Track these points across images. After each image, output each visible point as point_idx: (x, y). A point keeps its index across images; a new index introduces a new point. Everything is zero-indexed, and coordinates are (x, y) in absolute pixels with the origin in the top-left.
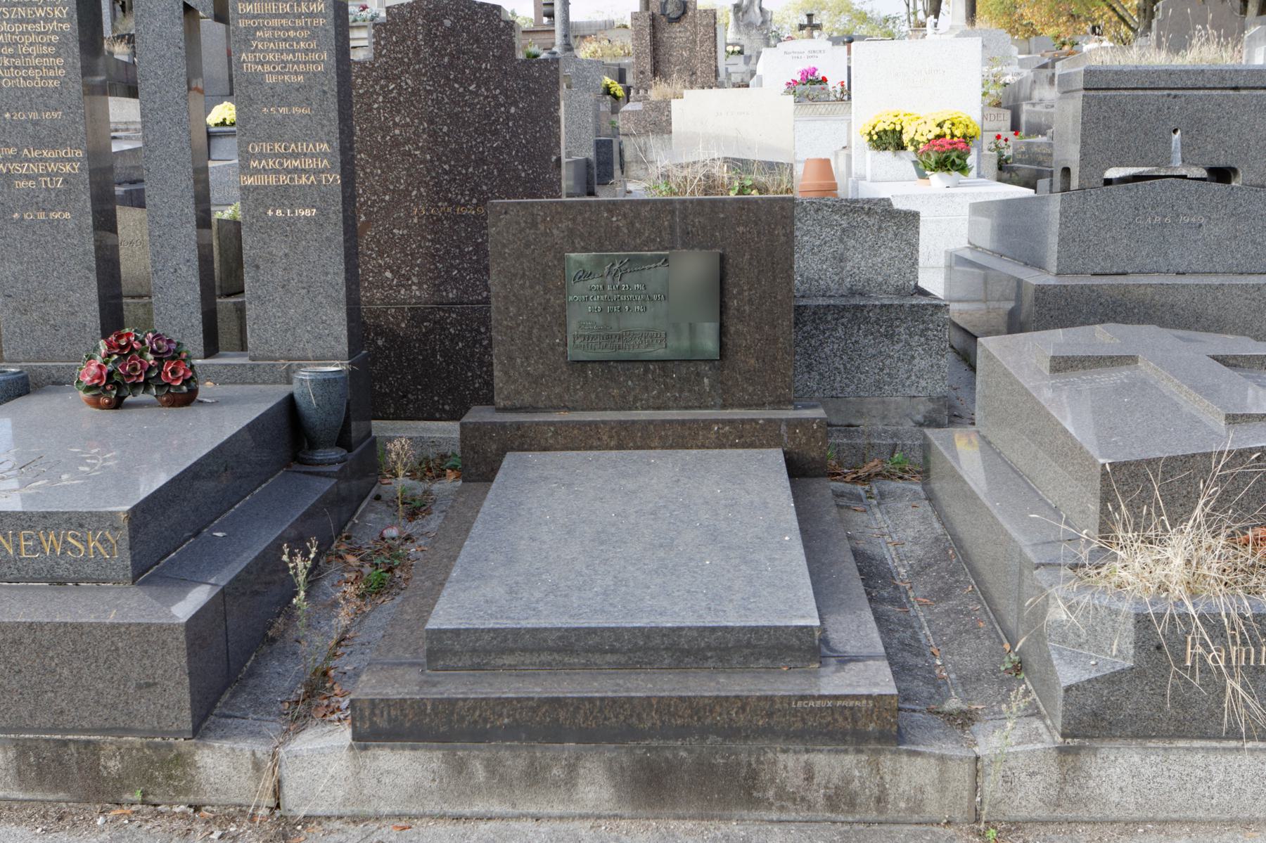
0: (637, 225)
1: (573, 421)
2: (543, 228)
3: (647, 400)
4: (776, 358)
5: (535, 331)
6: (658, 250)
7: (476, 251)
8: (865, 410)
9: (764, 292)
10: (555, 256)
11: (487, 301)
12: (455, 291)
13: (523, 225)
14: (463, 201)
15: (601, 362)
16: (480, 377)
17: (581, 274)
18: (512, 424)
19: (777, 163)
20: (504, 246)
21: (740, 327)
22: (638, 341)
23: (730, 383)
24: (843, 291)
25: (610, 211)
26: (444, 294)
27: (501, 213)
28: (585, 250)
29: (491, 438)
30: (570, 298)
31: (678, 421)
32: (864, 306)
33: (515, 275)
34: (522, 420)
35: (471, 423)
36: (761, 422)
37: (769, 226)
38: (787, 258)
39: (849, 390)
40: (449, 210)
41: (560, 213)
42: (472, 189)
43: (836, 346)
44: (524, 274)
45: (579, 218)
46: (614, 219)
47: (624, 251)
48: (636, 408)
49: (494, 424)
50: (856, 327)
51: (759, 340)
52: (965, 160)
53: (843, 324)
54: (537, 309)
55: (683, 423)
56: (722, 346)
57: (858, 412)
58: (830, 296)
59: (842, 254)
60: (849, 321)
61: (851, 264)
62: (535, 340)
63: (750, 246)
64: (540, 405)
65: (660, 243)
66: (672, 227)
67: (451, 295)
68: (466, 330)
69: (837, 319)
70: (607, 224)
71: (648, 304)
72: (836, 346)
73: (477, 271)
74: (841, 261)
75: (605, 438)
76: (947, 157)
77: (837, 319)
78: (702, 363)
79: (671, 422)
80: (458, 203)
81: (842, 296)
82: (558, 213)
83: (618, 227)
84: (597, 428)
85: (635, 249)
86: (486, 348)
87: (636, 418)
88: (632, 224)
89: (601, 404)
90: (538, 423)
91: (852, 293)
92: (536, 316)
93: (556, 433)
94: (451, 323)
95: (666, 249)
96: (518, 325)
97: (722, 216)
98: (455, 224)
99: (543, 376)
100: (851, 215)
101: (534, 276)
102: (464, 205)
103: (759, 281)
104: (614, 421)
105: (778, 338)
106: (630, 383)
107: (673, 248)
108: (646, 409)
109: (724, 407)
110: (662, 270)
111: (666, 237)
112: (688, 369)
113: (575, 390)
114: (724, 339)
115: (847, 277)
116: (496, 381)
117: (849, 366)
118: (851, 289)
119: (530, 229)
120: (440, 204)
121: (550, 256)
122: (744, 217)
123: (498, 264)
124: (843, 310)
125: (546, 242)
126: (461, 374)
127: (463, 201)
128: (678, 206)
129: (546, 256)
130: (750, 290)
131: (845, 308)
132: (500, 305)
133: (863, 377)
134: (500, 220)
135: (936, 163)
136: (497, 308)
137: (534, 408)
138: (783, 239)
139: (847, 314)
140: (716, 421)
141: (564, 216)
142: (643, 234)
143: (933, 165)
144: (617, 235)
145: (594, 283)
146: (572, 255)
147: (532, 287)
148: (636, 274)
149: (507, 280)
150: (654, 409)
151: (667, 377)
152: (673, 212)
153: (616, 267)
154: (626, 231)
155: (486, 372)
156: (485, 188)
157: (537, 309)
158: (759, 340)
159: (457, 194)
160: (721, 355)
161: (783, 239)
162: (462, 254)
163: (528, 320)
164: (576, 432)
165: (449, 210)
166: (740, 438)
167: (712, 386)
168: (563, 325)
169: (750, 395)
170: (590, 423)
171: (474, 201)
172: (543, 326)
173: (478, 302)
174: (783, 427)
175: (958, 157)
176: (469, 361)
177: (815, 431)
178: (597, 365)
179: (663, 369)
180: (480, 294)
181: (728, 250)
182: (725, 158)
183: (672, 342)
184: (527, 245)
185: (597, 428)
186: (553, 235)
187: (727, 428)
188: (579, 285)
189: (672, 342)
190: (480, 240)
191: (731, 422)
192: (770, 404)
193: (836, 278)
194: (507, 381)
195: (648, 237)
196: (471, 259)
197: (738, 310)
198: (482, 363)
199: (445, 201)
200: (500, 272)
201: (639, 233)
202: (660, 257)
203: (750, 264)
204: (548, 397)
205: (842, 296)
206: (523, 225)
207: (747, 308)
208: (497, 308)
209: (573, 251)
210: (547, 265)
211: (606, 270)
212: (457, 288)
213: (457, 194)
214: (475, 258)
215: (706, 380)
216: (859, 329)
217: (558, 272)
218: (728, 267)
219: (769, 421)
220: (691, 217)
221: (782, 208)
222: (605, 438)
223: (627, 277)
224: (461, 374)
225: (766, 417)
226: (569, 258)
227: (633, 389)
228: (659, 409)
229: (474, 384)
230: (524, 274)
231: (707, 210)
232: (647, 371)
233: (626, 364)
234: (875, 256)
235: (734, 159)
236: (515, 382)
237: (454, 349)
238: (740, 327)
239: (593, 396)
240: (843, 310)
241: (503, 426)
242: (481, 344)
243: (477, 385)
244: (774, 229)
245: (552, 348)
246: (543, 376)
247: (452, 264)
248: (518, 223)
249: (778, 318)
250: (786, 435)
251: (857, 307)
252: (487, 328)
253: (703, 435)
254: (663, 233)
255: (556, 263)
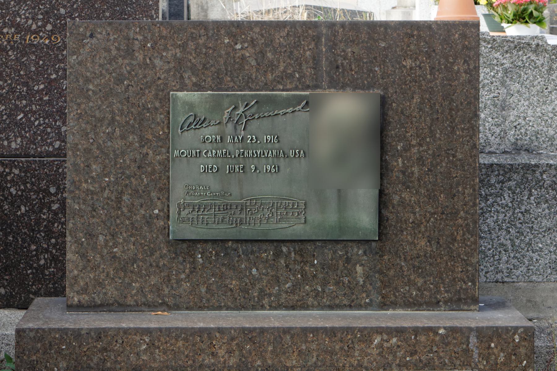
0: (269, 55)
1: (177, 329)
2: (141, 57)
3: (278, 296)
4: (455, 240)
5: (125, 198)
6: (296, 89)
7: (48, 90)
8: (538, 299)
9: (439, 148)
10: (157, 95)
11: (60, 153)
12: (19, 140)
13: (114, 52)
14: (34, 27)
15: (214, 241)
16: (47, 251)
17: (191, 120)
18: (89, 332)
19: (359, 11)
20: (88, 80)
21: (406, 195)
22: (267, 213)
23: (392, 273)
24: (506, 146)
25: (232, 36)
26: (6, 143)
27: (84, 36)
28: (198, 87)
29: (59, 352)
30: (176, 153)
31: (325, 329)
32: (536, 166)
33: (101, 120)
34: (104, 325)
35: (31, 330)
36: (441, 331)
37: (447, 60)
38: (469, 103)
39: (518, 272)
40: (17, 38)
41: (165, 38)
42: (47, 13)
43: (501, 217)
44: (113, 119)
45: (191, 45)
46: (238, 46)
47: (251, 90)
48: (263, 307)
49: (64, 331)
50: (526, 193)
51: (432, 214)
52: (542, 12)
53: (510, 189)
54: (129, 167)
55: (332, 332)
56: (382, 220)
57: (529, 301)
58: (490, 153)
59: (504, 101)
60: (518, 185)
61: (515, 112)
62: (125, 210)
63: (420, 87)
64: (130, 301)
65: (299, 79)
66: (316, 60)
67: (13, 145)
68: (30, 191)
69: (502, 182)
70: (228, 54)
71: (282, 163)
72: (501, 217)
73: (48, 115)
74: (504, 109)
75: (221, 352)
76: (525, 10)
77: (502, 182)
78: (354, 244)
79: (315, 330)
80: (28, 30)
81: (505, 152)
82: (161, 37)
83: (243, 58)
84: (210, 338)
85: (266, 87)
86: (56, 213)
87: (265, 325)
88: (262, 53)
89: (214, 301)
90: (126, 331)
91: (517, 149)
92: (129, 177)
93: (151, 345)
94: (12, 181)
95: (308, 87)
96: (103, 189)
97: (383, 45)
98: (23, 56)
99: (134, 260)
100: (515, 52)
101: (127, 123)
102: (36, 32)
103: (432, 134)
104: (235, 329)
105: (457, 213)
106: (254, 271)
107: (316, 87)
108: (275, 309)
109: (383, 306)
110: (303, 116)
111: (308, 72)
112: (335, 252)
113: (178, 281)
114: (385, 212)
115: (511, 129)
116: (69, 266)
117: (517, 242)
118: (515, 144)
119: (124, 58)
120: (5, 30)
121: (150, 95)
122: (412, 47)
123: (79, 105)
124: (510, 170)
125: (145, 77)
126: (22, 247)
127: (34, 27)
128: (324, 31)
129: (144, 94)
130: (420, 145)
131: (512, 168)
132: (78, 161)
133: (535, 256)
134: (84, 46)
135: (514, 15)
136: (75, 165)
137: (120, 305)
138: (464, 77)
139: (515, 176)
140: (379, 331)
141: (170, 42)
142: (278, 67)
143: (511, 17)
144: (242, 68)
145: (208, 132)
146: (180, 94)
147: (123, 137)
148: (266, 122)
149: (89, 127)
150: (287, 308)
151: (305, 263)
152: (317, 39)
153: (240, 111)
154: (253, 63)
155: (54, 246)
156: (62, 11)
157: (129, 167)
158: (432, 214)
159: (27, 18)
160: (380, 234)
161: (464, 77)
162: (31, 93)
163: (116, 183)
164: (180, 343)
165: (17, 38)
166: (412, 355)
167: (367, 277)
168: (165, 190)
169: (419, 289)
170: (201, 332)
171: (49, 27)
172: (137, 191)
173: (49, 155)
174: (473, 340)
175: (536, 9)
176: (33, 230)
177: (517, 346)
178: (209, 247)
179: (300, 253)
180: (51, 144)
181: (391, 90)
182: (306, 6)
183: (314, 216)
184: (119, 80)
185: (210, 338)
186: (154, 67)
187: (394, 340)
188: (189, 135)
189: (314, 216)
190: (54, 76)
191: (400, 331)
192: (446, 303)
193: (498, 131)
194: (85, 268)
195: (284, 71)
196: (41, 99)
197: (404, 173)
198: (49, 233)
199: (12, 26)
200: (80, 116)
201: (272, 66)
202: (299, 99)
203: (421, 110)
204: (141, 290)
205: (505, 152)
206: (114, 52)
207: (416, 169)
208: (75, 165)
209: (181, 90)
210: (145, 107)
211: (226, 116)
212: (22, 136)
213: (27, 18)
214: (46, 98)
215: (359, 269)
216: (531, 195)
217: (160, 117)
218: (390, 113)
219: (453, 330)
220: (342, 46)
221: (464, 36)
222: (221, 352)
223: (254, 125)
224: (22, 247)
225: (448, 324)
226: (176, 99)
227: (260, 280)
228: (293, 308)
229: (39, 260)
230: (113, 119)
231: (364, 36)
232: (278, 254)
233: (249, 245)
234: (544, 103)
235: (315, 7)
236: (95, 268)
237: (15, 214)
238: (406, 195)
239: (203, 290)
240: (510, 170)
241: (77, 334)
242: (49, 208)
243: (42, 262)
244: (453, 64)
245: (149, 221)
246: (134, 260)
247: (16, 106)
248: (108, 51)
249: (458, 184)
250: (476, 351)
251: (527, 167)
252: (58, 188)
253: (361, 350)
254: (304, 67)
255: (157, 104)
